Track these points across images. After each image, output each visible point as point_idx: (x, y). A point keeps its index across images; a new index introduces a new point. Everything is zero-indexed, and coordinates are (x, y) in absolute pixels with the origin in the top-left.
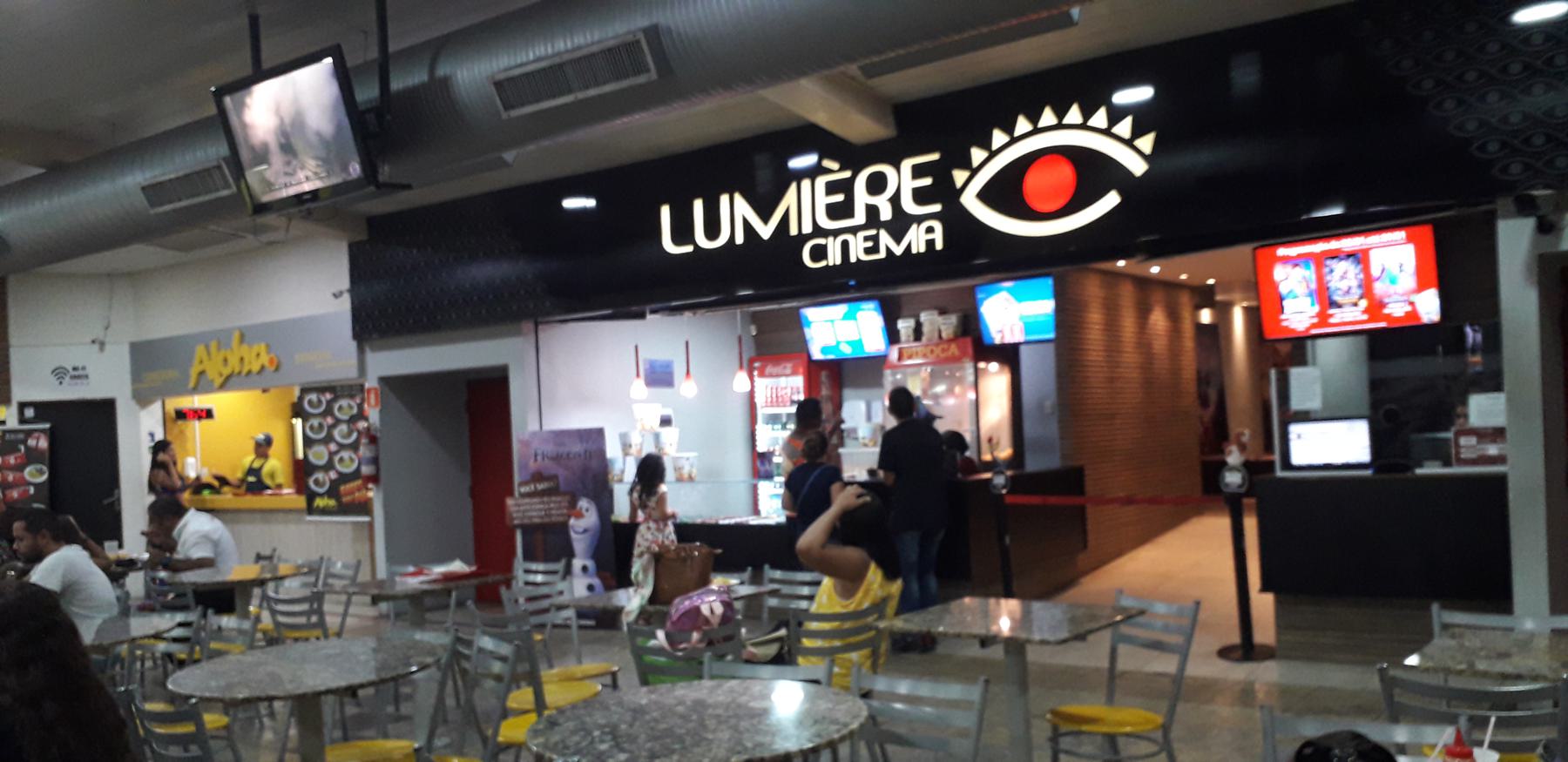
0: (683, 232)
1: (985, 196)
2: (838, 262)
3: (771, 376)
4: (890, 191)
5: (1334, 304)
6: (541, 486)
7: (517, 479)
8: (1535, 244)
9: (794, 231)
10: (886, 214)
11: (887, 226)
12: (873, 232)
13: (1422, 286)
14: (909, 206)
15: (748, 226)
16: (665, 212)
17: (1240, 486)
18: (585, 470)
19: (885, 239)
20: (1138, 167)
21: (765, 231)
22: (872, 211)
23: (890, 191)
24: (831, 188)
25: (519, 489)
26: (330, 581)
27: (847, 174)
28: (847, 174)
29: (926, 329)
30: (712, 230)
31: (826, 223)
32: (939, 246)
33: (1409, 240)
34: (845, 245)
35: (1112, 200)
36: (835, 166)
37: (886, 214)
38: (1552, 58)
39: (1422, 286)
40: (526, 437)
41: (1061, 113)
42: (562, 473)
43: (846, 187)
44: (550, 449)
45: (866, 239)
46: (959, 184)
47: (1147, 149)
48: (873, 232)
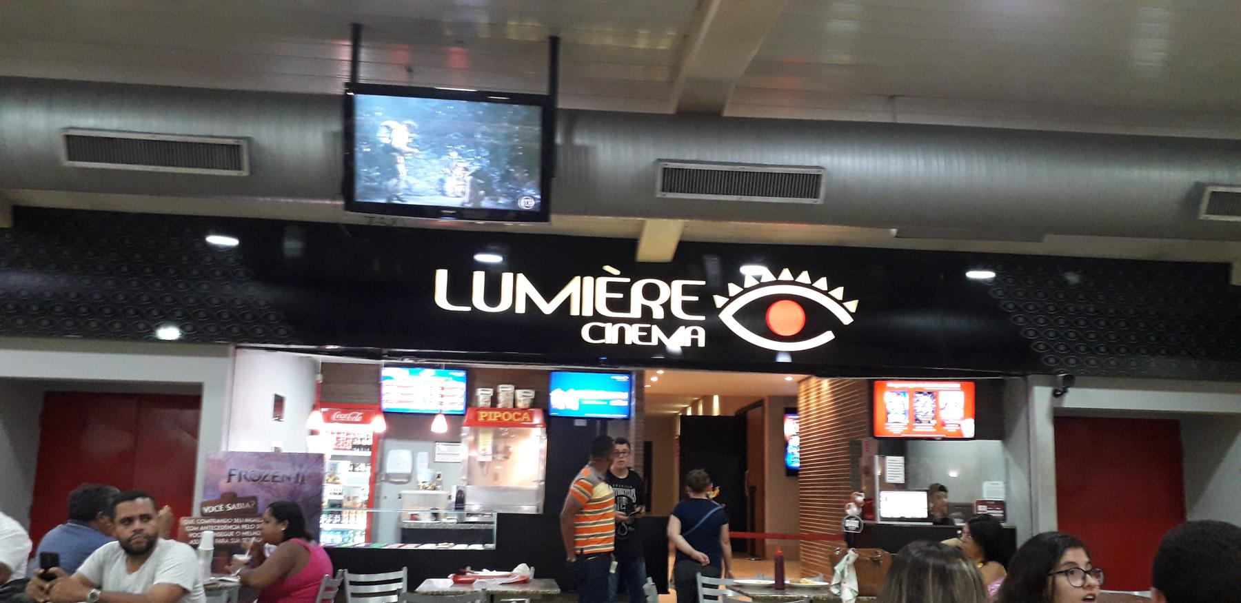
0: (459, 291)
1: (738, 316)
2: (615, 341)
4: (663, 299)
6: (229, 508)
7: (198, 498)
8: (1052, 402)
9: (575, 311)
10: (658, 314)
14: (677, 311)
15: (529, 300)
16: (442, 277)
19: (657, 333)
20: (847, 320)
21: (548, 308)
22: (647, 311)
23: (663, 299)
24: (611, 287)
25: (196, 511)
27: (628, 280)
28: (628, 280)
29: (501, 398)
30: (493, 294)
31: (604, 311)
32: (702, 343)
33: (962, 388)
34: (622, 332)
35: (828, 336)
36: (617, 272)
37: (658, 314)
38: (764, 305)
39: (965, 417)
40: (220, 456)
43: (625, 289)
44: (251, 470)
46: (719, 305)
47: (853, 310)
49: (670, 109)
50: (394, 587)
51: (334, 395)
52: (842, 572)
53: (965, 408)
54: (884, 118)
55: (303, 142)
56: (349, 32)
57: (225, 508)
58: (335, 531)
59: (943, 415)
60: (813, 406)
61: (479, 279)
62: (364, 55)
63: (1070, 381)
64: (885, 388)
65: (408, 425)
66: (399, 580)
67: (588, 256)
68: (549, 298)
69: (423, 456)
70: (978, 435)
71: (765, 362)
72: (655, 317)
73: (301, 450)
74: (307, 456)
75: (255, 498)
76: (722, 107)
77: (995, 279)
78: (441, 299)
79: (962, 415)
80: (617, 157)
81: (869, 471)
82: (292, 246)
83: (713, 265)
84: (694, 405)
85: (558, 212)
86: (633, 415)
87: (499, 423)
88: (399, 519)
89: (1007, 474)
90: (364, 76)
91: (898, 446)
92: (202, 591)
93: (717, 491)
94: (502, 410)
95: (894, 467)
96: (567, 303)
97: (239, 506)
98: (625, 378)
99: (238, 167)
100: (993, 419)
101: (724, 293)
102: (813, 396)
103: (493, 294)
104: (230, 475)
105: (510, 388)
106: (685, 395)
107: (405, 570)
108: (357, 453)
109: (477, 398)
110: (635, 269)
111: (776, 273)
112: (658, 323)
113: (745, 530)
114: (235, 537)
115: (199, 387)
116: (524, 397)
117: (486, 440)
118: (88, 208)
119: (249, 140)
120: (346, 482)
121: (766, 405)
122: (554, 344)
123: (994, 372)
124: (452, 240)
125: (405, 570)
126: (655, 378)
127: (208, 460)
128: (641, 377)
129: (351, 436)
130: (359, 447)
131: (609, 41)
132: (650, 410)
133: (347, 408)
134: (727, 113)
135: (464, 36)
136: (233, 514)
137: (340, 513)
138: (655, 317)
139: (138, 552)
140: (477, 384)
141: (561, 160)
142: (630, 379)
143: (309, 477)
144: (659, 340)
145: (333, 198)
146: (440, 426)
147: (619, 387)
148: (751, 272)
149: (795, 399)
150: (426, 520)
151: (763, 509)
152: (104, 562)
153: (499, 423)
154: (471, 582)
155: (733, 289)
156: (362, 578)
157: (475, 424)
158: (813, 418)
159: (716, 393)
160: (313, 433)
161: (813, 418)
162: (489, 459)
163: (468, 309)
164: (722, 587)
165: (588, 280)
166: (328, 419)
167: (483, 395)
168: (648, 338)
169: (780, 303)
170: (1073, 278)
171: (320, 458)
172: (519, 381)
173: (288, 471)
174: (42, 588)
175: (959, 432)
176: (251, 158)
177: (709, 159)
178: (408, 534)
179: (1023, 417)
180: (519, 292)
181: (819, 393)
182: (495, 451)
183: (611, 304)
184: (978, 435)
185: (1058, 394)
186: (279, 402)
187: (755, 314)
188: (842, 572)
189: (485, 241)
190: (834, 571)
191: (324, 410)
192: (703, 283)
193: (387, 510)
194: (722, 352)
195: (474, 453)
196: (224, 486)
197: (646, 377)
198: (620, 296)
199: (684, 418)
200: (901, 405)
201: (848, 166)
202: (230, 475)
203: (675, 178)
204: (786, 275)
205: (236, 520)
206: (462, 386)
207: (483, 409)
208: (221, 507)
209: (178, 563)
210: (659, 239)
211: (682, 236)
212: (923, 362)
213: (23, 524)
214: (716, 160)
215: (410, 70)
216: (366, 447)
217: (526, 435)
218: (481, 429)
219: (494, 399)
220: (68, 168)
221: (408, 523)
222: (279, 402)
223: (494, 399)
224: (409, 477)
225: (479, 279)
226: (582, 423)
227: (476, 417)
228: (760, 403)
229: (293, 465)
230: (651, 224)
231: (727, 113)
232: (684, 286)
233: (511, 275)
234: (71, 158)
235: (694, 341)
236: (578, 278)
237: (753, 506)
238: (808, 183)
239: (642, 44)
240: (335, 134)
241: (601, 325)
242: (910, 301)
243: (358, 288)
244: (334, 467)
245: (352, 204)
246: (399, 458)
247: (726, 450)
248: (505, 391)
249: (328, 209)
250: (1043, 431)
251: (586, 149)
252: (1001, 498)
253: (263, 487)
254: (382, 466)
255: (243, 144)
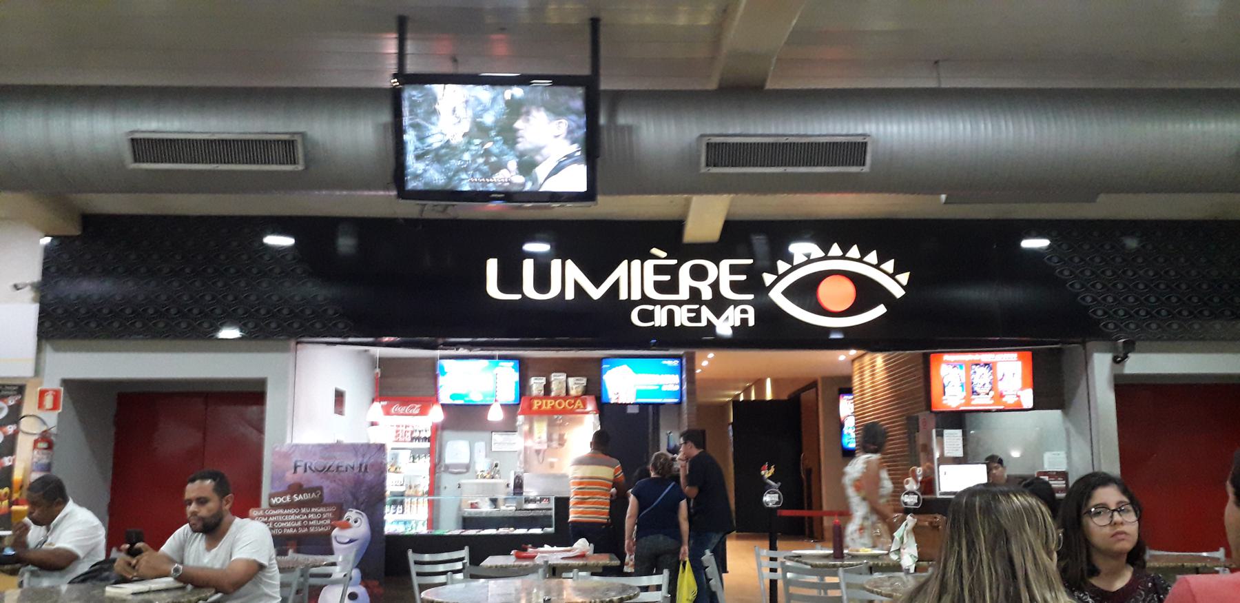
0: (510, 280)
1: (787, 293)
2: (664, 323)
3: (397, 414)
4: (711, 279)
5: (974, 392)
6: (296, 498)
7: (266, 489)
8: (1112, 369)
9: (623, 295)
10: (707, 294)
11: (708, 304)
12: (696, 307)
13: (1024, 387)
14: (726, 292)
15: (578, 287)
16: (492, 266)
17: (916, 504)
18: (358, 483)
19: (706, 313)
20: (898, 292)
21: (596, 293)
22: (695, 294)
23: (711, 279)
24: (658, 270)
26: (792, 590)
27: (674, 262)
28: (674, 262)
29: (554, 386)
30: (542, 282)
31: (652, 294)
32: (751, 323)
33: (1019, 359)
34: (671, 314)
35: (880, 310)
36: (664, 254)
37: (707, 294)
38: (815, 280)
39: (1024, 387)
40: (284, 449)
41: (845, 249)
42: (328, 486)
43: (673, 271)
44: (316, 462)
45: (690, 311)
46: (768, 283)
47: (905, 283)
48: (696, 307)
49: (712, 85)
50: (459, 566)
51: (394, 387)
52: (902, 539)
53: (1024, 378)
54: (932, 84)
55: (355, 134)
56: (394, 25)
57: (292, 498)
58: (398, 522)
59: (1001, 386)
60: (867, 384)
61: (528, 266)
62: (410, 47)
63: (1130, 347)
64: (940, 362)
65: (466, 416)
66: (461, 559)
67: (633, 239)
68: (597, 284)
69: (480, 446)
70: (1036, 406)
71: (818, 339)
72: (704, 298)
73: (363, 441)
74: (369, 446)
75: (321, 488)
76: (764, 81)
77: (1050, 246)
78: (492, 289)
79: (1020, 385)
80: (660, 135)
81: (928, 450)
82: (346, 244)
83: (759, 242)
84: (747, 391)
85: (604, 194)
86: (685, 399)
87: (553, 411)
88: (460, 508)
89: (1068, 441)
90: (411, 68)
91: (957, 419)
92: (276, 568)
93: (772, 470)
94: (556, 398)
95: (953, 441)
96: (616, 285)
97: (306, 496)
98: (675, 363)
99: (294, 162)
100: (1052, 389)
101: (773, 270)
102: (867, 373)
103: (542, 282)
104: (296, 468)
105: (563, 377)
106: (736, 380)
107: (467, 548)
108: (416, 445)
109: (531, 387)
110: (682, 251)
111: (826, 248)
112: (706, 303)
113: (802, 508)
114: (302, 527)
115: (262, 383)
116: (576, 385)
117: (541, 429)
118: (149, 212)
119: (303, 134)
120: (406, 473)
121: (820, 385)
122: (607, 328)
123: (1054, 342)
124: (498, 228)
125: (467, 548)
126: (707, 360)
127: (274, 453)
128: (691, 360)
129: (410, 429)
130: (418, 439)
131: (649, 19)
132: (702, 398)
133: (405, 401)
134: (769, 85)
135: (505, 23)
136: (301, 504)
137: (402, 503)
138: (704, 298)
139: (212, 530)
140: (530, 373)
141: (605, 139)
142: (681, 363)
143: (372, 465)
144: (709, 321)
145: (386, 188)
146: (496, 415)
147: (671, 370)
148: (800, 249)
149: (849, 379)
150: (486, 508)
151: (820, 489)
152: (185, 541)
153: (553, 411)
154: (533, 557)
155: (782, 266)
156: (427, 557)
157: (530, 412)
158: (868, 396)
159: (769, 373)
160: (373, 424)
161: (868, 396)
162: (545, 447)
163: (518, 297)
164: (780, 560)
165: (636, 264)
166: (387, 412)
167: (536, 384)
168: (697, 318)
169: (833, 278)
170: (1132, 243)
171: (381, 448)
172: (571, 368)
173: (351, 461)
174: (129, 564)
175: (1019, 403)
176: (306, 155)
177: (752, 132)
178: (467, 522)
179: (1082, 390)
180: (568, 278)
181: (873, 370)
182: (550, 439)
183: (659, 287)
184: (1036, 406)
185: (1118, 360)
186: (339, 396)
187: (805, 291)
188: (902, 539)
189: (534, 229)
190: (893, 538)
191: (384, 403)
192: (750, 261)
193: (447, 497)
194: (771, 331)
195: (529, 443)
196: (290, 477)
197: (697, 362)
198: (667, 278)
199: (736, 403)
200: (958, 378)
201: (894, 133)
202: (296, 468)
203: (720, 153)
204: (835, 250)
205: (303, 510)
206: (516, 376)
207: (538, 398)
208: (288, 498)
209: (250, 539)
210: (705, 218)
211: (728, 214)
212: (977, 334)
213: (101, 519)
214: (760, 132)
215: (455, 60)
216: (425, 439)
217: (580, 422)
218: (536, 417)
219: (547, 388)
220: (134, 170)
221: (469, 511)
222: (339, 396)
223: (547, 388)
224: (467, 467)
225: (528, 266)
226: (635, 410)
227: (531, 406)
228: (813, 385)
229: (356, 455)
230: (697, 201)
231: (769, 85)
232: (731, 266)
233: (559, 261)
234: (136, 160)
235: (744, 321)
236: (626, 262)
237: (809, 487)
238: (854, 151)
239: (682, 20)
240: (385, 126)
241: (650, 307)
242: (963, 273)
243: (414, 278)
244: (395, 457)
245: (404, 194)
246: (457, 449)
247: (781, 434)
248: (558, 379)
249: (378, 202)
250: (1105, 398)
251: (630, 129)
252: (1063, 468)
253: (328, 478)
254: (440, 461)
255: (298, 139)
